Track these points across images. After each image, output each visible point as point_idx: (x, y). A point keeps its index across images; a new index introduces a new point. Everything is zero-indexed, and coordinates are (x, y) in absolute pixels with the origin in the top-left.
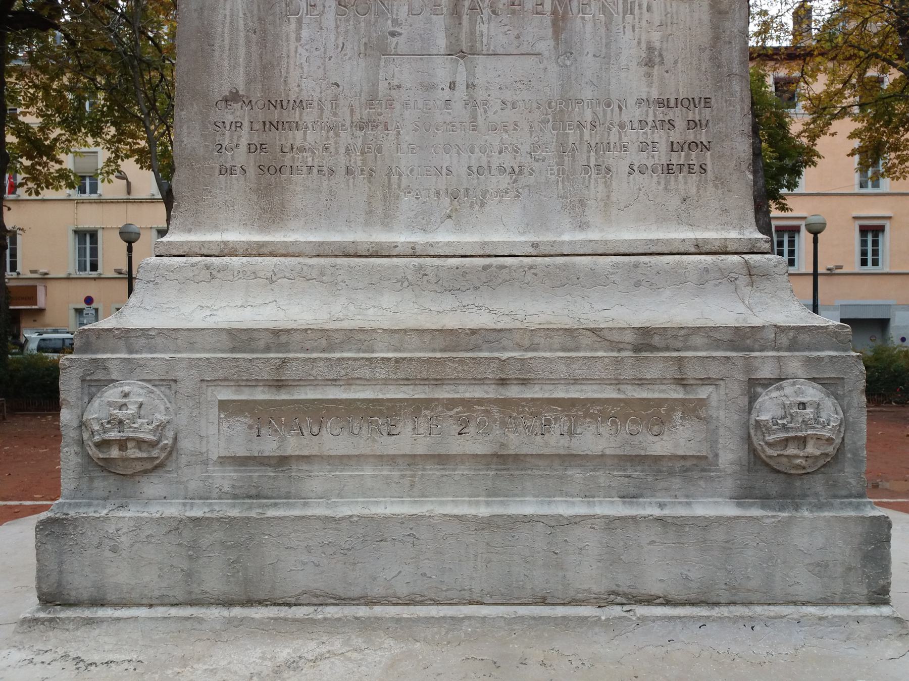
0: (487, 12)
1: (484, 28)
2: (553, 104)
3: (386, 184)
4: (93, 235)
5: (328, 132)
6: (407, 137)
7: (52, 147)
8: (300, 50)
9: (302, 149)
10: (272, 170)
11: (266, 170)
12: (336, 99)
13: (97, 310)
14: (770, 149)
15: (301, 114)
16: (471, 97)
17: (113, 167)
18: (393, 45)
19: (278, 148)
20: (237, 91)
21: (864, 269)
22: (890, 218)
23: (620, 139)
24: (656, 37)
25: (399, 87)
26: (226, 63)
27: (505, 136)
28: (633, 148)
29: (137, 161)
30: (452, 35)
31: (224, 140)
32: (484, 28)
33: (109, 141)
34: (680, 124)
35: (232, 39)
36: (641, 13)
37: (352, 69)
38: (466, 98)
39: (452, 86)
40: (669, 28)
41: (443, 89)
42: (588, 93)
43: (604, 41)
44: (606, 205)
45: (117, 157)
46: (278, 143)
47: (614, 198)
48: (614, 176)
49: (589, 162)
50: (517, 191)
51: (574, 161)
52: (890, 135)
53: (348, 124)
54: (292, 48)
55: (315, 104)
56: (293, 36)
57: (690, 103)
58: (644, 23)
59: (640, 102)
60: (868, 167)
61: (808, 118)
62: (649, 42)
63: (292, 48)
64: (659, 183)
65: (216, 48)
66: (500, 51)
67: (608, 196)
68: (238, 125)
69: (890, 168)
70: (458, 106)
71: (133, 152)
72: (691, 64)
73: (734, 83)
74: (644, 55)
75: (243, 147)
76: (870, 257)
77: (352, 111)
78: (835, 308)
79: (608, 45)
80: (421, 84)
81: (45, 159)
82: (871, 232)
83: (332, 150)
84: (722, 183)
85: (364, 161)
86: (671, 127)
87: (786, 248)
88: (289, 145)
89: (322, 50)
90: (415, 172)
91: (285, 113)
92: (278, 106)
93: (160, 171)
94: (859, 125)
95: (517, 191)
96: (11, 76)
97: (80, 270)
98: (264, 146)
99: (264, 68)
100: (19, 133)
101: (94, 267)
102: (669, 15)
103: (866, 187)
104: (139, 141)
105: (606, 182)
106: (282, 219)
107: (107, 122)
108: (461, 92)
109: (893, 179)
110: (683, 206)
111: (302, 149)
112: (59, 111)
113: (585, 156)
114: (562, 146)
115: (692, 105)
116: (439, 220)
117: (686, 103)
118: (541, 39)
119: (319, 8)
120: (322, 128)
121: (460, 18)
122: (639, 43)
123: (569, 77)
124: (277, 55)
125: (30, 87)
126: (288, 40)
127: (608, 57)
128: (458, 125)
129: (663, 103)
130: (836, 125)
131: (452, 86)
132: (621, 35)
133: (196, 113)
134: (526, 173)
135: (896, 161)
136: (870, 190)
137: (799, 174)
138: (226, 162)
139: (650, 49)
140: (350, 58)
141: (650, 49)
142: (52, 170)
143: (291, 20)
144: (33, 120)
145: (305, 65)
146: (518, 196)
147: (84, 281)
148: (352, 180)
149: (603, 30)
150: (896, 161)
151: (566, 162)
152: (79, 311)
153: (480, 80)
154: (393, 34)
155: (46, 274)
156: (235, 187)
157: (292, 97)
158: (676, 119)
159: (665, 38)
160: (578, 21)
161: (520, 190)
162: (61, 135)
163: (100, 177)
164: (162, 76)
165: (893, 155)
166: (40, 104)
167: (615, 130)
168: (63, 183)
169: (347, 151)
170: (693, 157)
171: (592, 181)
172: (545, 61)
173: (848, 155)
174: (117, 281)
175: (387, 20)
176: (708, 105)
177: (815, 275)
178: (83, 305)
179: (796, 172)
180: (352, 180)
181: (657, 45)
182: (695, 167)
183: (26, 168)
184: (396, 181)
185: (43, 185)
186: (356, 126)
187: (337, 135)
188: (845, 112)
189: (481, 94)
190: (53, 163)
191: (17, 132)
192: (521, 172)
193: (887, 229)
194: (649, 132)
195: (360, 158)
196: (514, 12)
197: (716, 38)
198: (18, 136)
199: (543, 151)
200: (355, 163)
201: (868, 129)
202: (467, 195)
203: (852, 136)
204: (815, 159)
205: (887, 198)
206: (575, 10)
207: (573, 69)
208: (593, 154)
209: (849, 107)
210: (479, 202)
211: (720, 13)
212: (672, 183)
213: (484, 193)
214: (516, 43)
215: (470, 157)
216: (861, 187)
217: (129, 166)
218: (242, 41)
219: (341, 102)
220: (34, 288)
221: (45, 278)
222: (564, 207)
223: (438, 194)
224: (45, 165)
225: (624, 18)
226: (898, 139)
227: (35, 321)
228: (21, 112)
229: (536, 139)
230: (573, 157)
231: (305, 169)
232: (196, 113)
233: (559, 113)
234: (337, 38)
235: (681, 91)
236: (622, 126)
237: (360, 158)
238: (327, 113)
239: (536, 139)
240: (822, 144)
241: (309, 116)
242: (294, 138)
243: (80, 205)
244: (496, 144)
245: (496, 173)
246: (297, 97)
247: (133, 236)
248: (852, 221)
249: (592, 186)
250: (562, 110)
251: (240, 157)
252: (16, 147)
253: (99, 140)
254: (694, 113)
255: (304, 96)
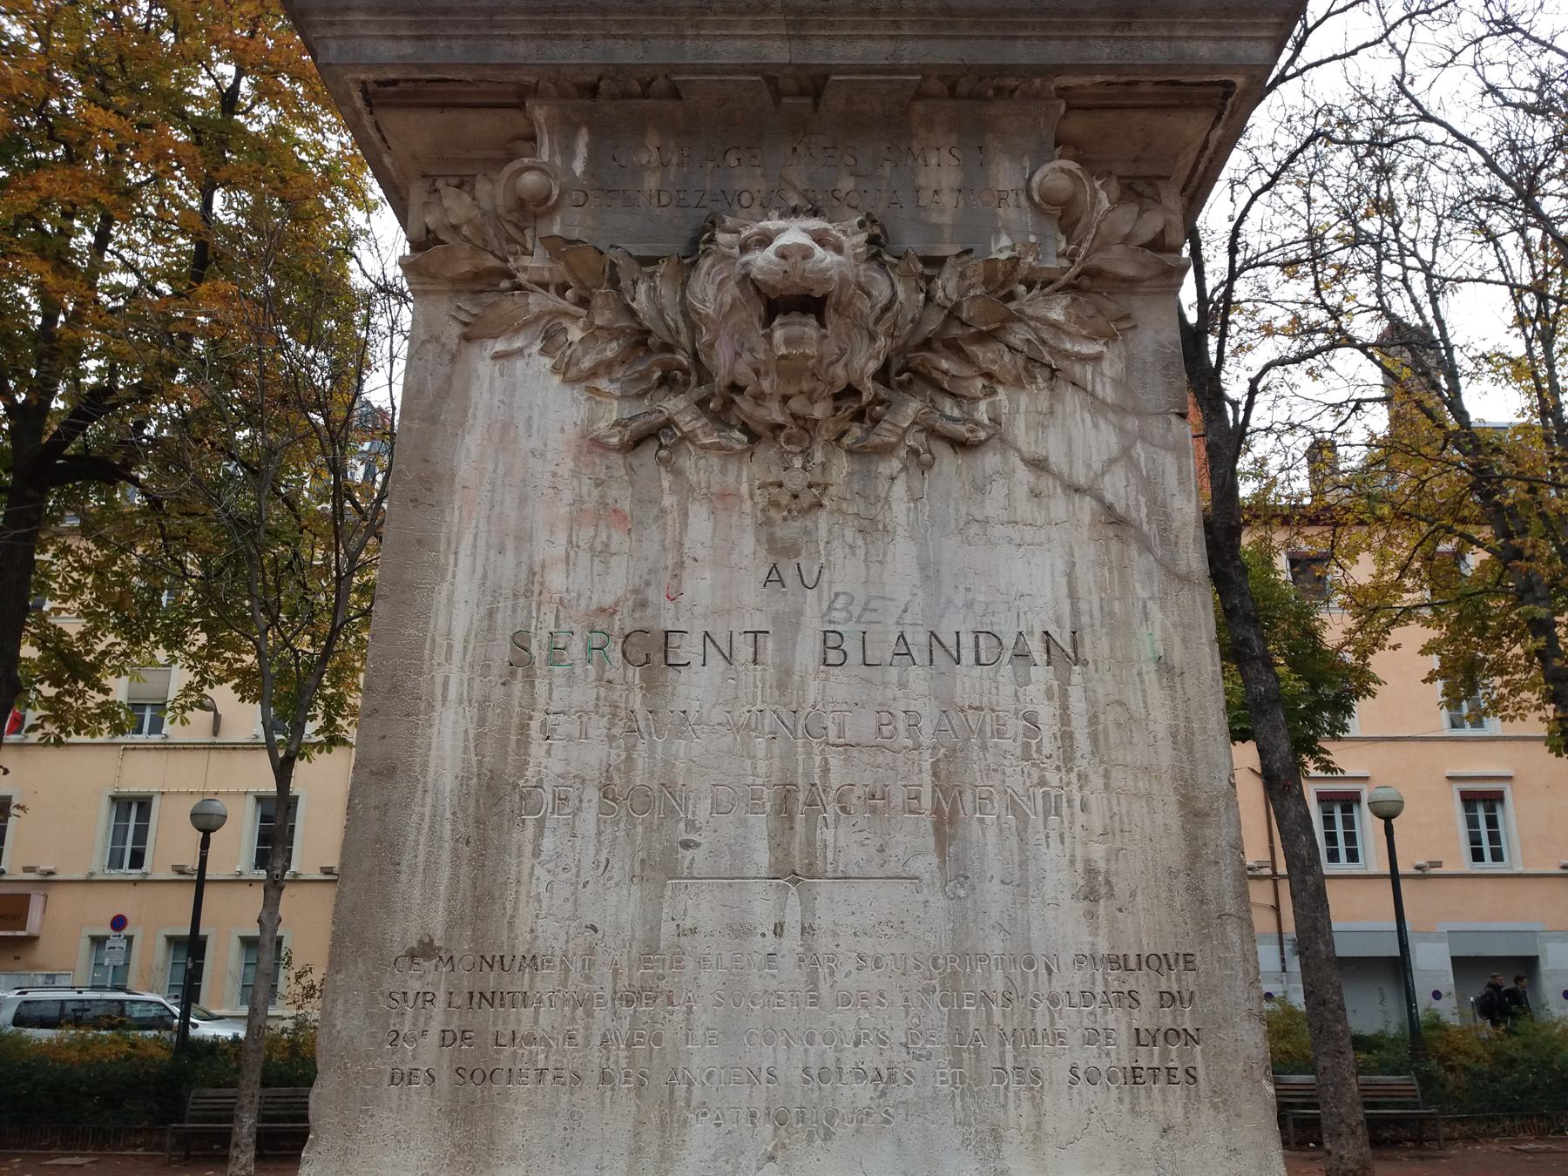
0: (832, 808)
1: (829, 834)
2: (941, 961)
3: (666, 1100)
4: (144, 804)
5: (575, 1008)
6: (703, 1018)
7: (95, 667)
8: (538, 871)
9: (530, 1040)
10: (478, 1076)
11: (468, 1077)
12: (591, 950)
13: (130, 939)
14: (1293, 676)
15: (532, 979)
16: (809, 949)
17: (194, 699)
18: (687, 863)
19: (491, 1037)
20: (432, 941)
21: (1478, 868)
22: (1509, 778)
23: (1052, 1023)
24: (1098, 852)
25: (694, 931)
26: (417, 892)
27: (864, 1015)
28: (1074, 1039)
29: (236, 688)
30: (780, 845)
31: (402, 1023)
32: (829, 834)
33: (193, 656)
34: (1148, 999)
35: (429, 853)
36: (1072, 814)
37: (620, 902)
38: (801, 949)
39: (779, 930)
40: (1118, 837)
41: (763, 935)
42: (995, 944)
43: (1016, 858)
44: (1036, 1139)
45: (204, 681)
46: (491, 1029)
47: (1048, 1126)
48: (1047, 1086)
49: (1003, 1062)
50: (886, 1112)
51: (978, 1060)
52: (1488, 651)
53: (608, 995)
54: (526, 870)
55: (557, 961)
56: (528, 848)
57: (1159, 963)
58: (1077, 828)
59: (1079, 960)
60: (1460, 700)
61: (1351, 623)
62: (1087, 861)
63: (526, 870)
64: (1121, 1100)
65: (404, 868)
66: (856, 872)
67: (1039, 1123)
68: (427, 998)
69: (1495, 702)
70: (787, 963)
71: (232, 672)
72: (1157, 897)
73: (1229, 929)
74: (1081, 882)
75: (433, 1038)
76: (1486, 847)
77: (616, 972)
78: (1439, 937)
79: (1023, 864)
80: (729, 926)
81: (81, 685)
82: (1482, 803)
83: (579, 1039)
84: (1225, 1102)
85: (631, 1059)
86: (1134, 1004)
87: (1342, 847)
88: (508, 1033)
89: (574, 870)
90: (715, 1078)
91: (506, 976)
92: (497, 966)
93: (274, 704)
94: (1433, 634)
95: (886, 1112)
96: (44, 551)
97: (111, 866)
98: (467, 1035)
99: (479, 900)
100: (44, 642)
101: (137, 860)
102: (1116, 818)
103: (1463, 726)
104: (244, 656)
105: (1033, 1097)
106: (488, 1165)
107: (195, 625)
108: (792, 940)
109: (1503, 719)
110: (1165, 1143)
111: (530, 1040)
112: (117, 607)
113: (996, 1051)
114: (958, 1033)
115: (1165, 966)
116: (754, 1164)
117: (1154, 962)
118: (917, 854)
119: (574, 803)
120: (565, 1002)
121: (791, 818)
122: (1072, 862)
123: (964, 917)
124: (500, 880)
125: (74, 569)
126: (519, 856)
127: (1023, 884)
128: (787, 995)
129: (1118, 962)
130: (1397, 634)
131: (779, 930)
132: (1043, 849)
133: (361, 977)
134: (901, 1081)
135: (1505, 691)
136: (1469, 731)
137: (1349, 710)
138: (403, 1062)
139: (1090, 872)
140: (617, 884)
141: (1090, 872)
142: (90, 704)
143: (528, 823)
144: (73, 626)
145: (545, 896)
146: (888, 1122)
147: (115, 887)
148: (609, 1094)
149: (1014, 840)
150: (1505, 691)
151: (966, 1062)
152: (98, 942)
153: (823, 920)
154: (686, 845)
155: (51, 873)
156: (415, 1108)
157: (521, 950)
158: (1141, 991)
159: (1114, 855)
160: (975, 825)
161: (891, 1111)
162: (113, 644)
163: (170, 714)
164: (296, 555)
165: (1498, 681)
166: (86, 597)
167: (1043, 1006)
168: (105, 725)
169: (604, 1041)
170: (1174, 1055)
171: (1011, 1095)
172: (925, 890)
173: (1424, 681)
174: (175, 886)
175: (678, 822)
176: (1190, 966)
177: (1395, 877)
178: (108, 931)
179: (1342, 707)
180: (609, 1094)
181: (1102, 865)
182: (1178, 1073)
183: (47, 699)
184: (684, 1094)
185: (71, 729)
186: (621, 999)
187: (589, 1014)
188: (1408, 613)
189: (824, 944)
190: (93, 693)
191: (41, 642)
192: (892, 1078)
193: (1508, 796)
194: (1099, 1011)
195: (625, 1053)
196: (874, 810)
197: (1194, 856)
198: (42, 648)
199: (927, 1041)
200: (617, 1062)
201: (1451, 640)
202: (802, 1118)
203: (1426, 650)
204: (1372, 686)
205: (1498, 744)
206: (969, 807)
207: (969, 903)
208: (1009, 1047)
209: (1416, 607)
210: (822, 1131)
211: (1196, 815)
212: (1143, 1101)
213: (831, 1116)
214: (878, 859)
215: (806, 1050)
216: (1454, 726)
217: (223, 695)
218: (446, 856)
219: (600, 957)
220: (26, 898)
221: (48, 881)
222: (965, 1142)
223: (753, 1115)
224: (82, 694)
225: (1045, 821)
226: (1503, 656)
227: (17, 958)
228: (53, 609)
229: (916, 1020)
230: (977, 1051)
231: (532, 1073)
232: (361, 977)
233: (950, 975)
234: (598, 851)
235: (1144, 942)
236: (1054, 1001)
237: (625, 1053)
238: (575, 976)
239: (916, 1020)
240: (1378, 663)
241: (546, 982)
242: (519, 1021)
243: (129, 753)
244: (850, 1029)
245: (851, 1079)
246: (528, 951)
247: (214, 821)
248: (1446, 783)
249: (1011, 1105)
250: (955, 973)
251: (427, 1053)
252: (37, 667)
253: (177, 653)
254: (1169, 979)
255: (540, 948)
